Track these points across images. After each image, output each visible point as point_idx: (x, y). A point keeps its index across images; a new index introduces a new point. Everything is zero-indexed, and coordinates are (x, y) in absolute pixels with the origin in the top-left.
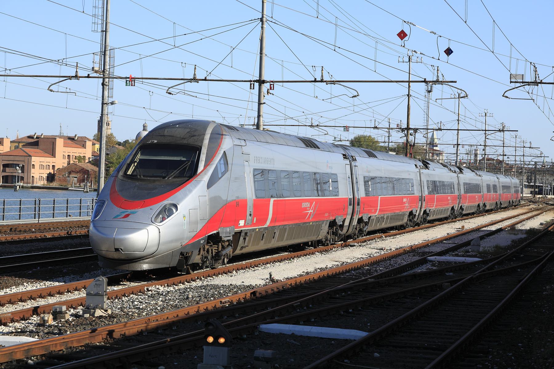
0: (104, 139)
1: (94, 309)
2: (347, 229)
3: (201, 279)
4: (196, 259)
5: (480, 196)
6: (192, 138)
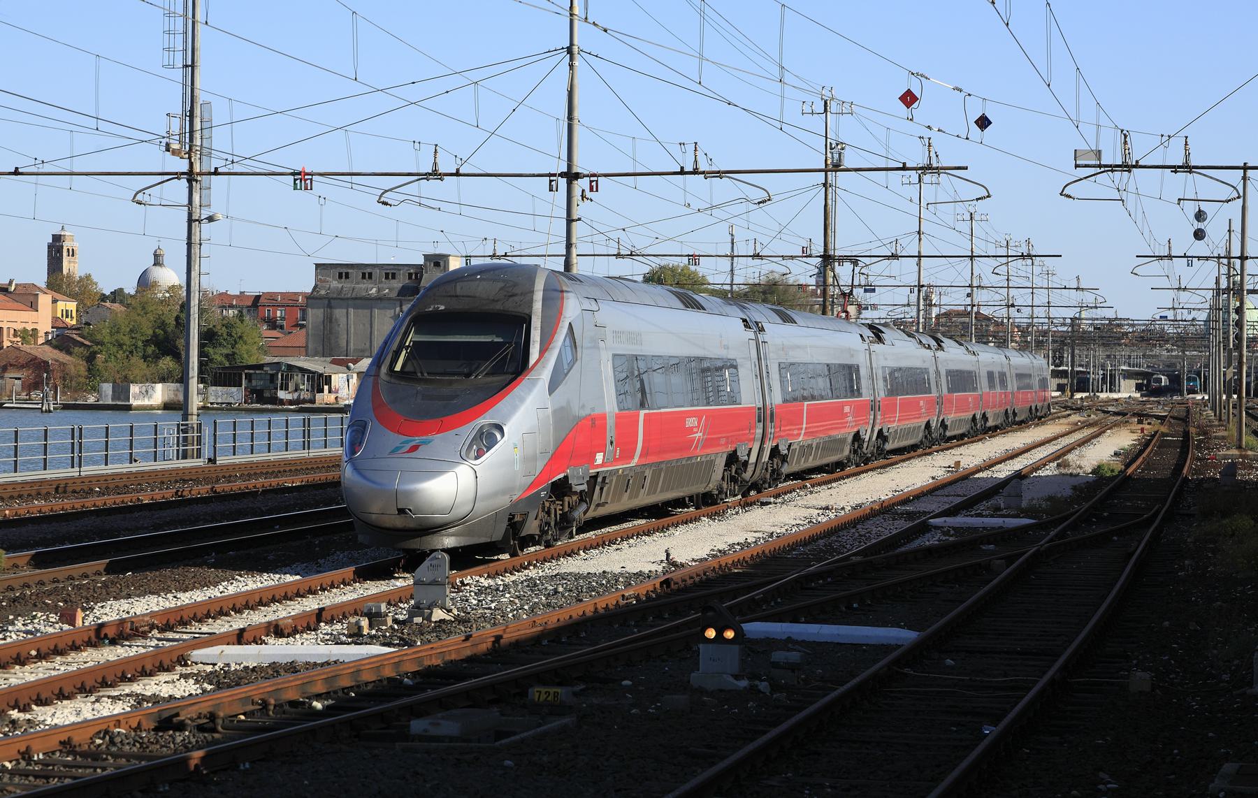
0: (194, 296)
1: (429, 609)
2: (753, 469)
3: (535, 566)
4: (532, 527)
5: (975, 398)
6: (511, 299)
